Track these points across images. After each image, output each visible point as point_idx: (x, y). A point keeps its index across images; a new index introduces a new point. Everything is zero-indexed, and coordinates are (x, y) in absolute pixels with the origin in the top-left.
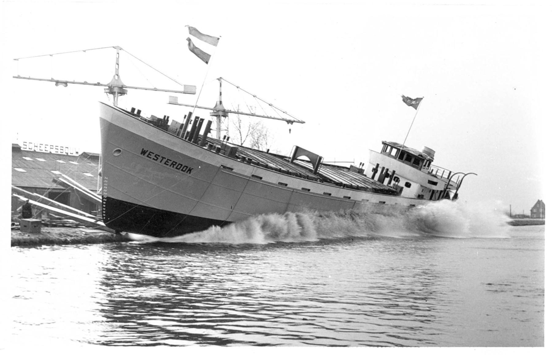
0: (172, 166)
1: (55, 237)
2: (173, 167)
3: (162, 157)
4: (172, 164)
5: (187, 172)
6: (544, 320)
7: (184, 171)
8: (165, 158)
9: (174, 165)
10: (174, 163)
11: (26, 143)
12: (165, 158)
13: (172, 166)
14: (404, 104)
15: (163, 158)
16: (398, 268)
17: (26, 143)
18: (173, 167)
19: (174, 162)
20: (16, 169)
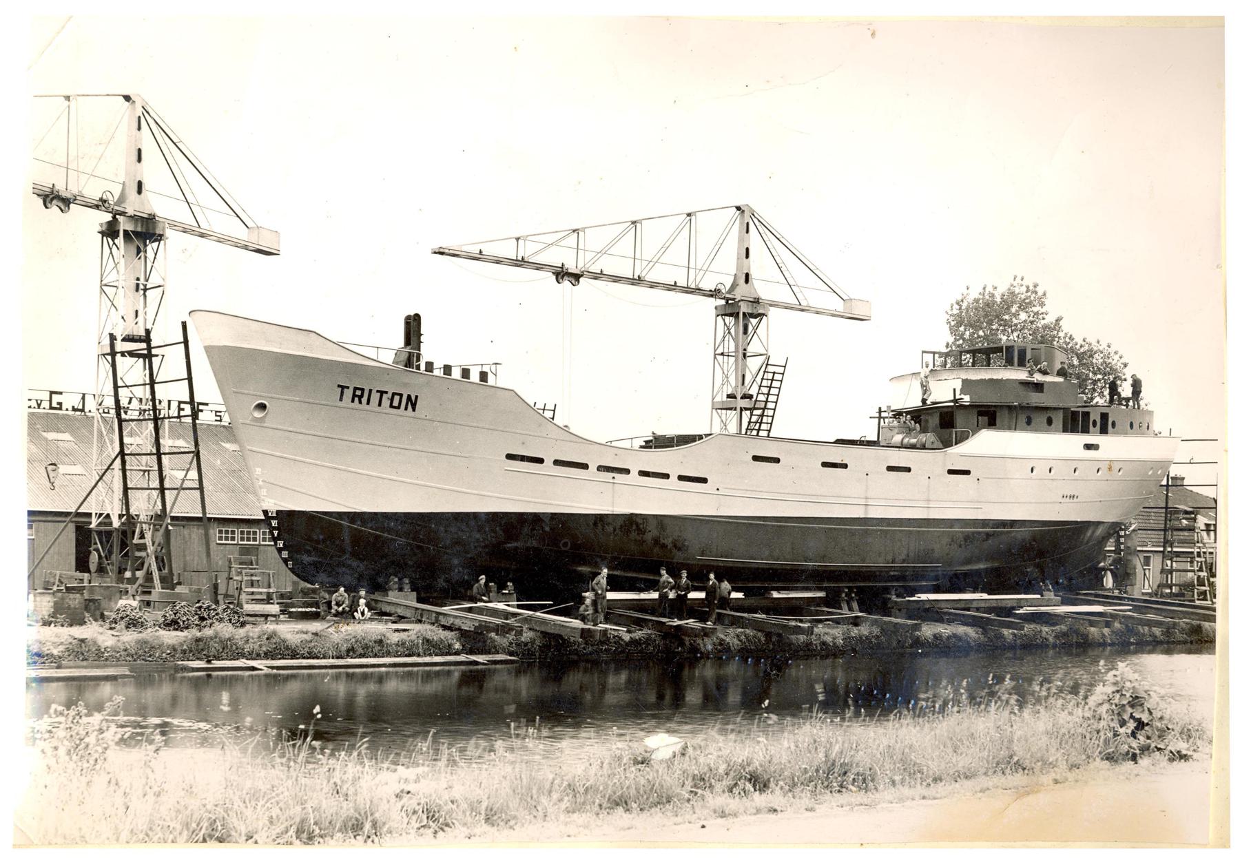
0: (356, 399)
1: (921, 502)
2: (360, 402)
3: (378, 391)
4: (354, 395)
5: (406, 409)
6: (1003, 428)
7: (398, 407)
8: (386, 392)
9: (360, 397)
10: (358, 393)
11: (954, 390)
12: (386, 392)
13: (356, 399)
14: (1217, 593)
15: (382, 393)
16: (212, 578)
17: (954, 390)
18: (360, 402)
19: (356, 389)
20: (1039, 596)
